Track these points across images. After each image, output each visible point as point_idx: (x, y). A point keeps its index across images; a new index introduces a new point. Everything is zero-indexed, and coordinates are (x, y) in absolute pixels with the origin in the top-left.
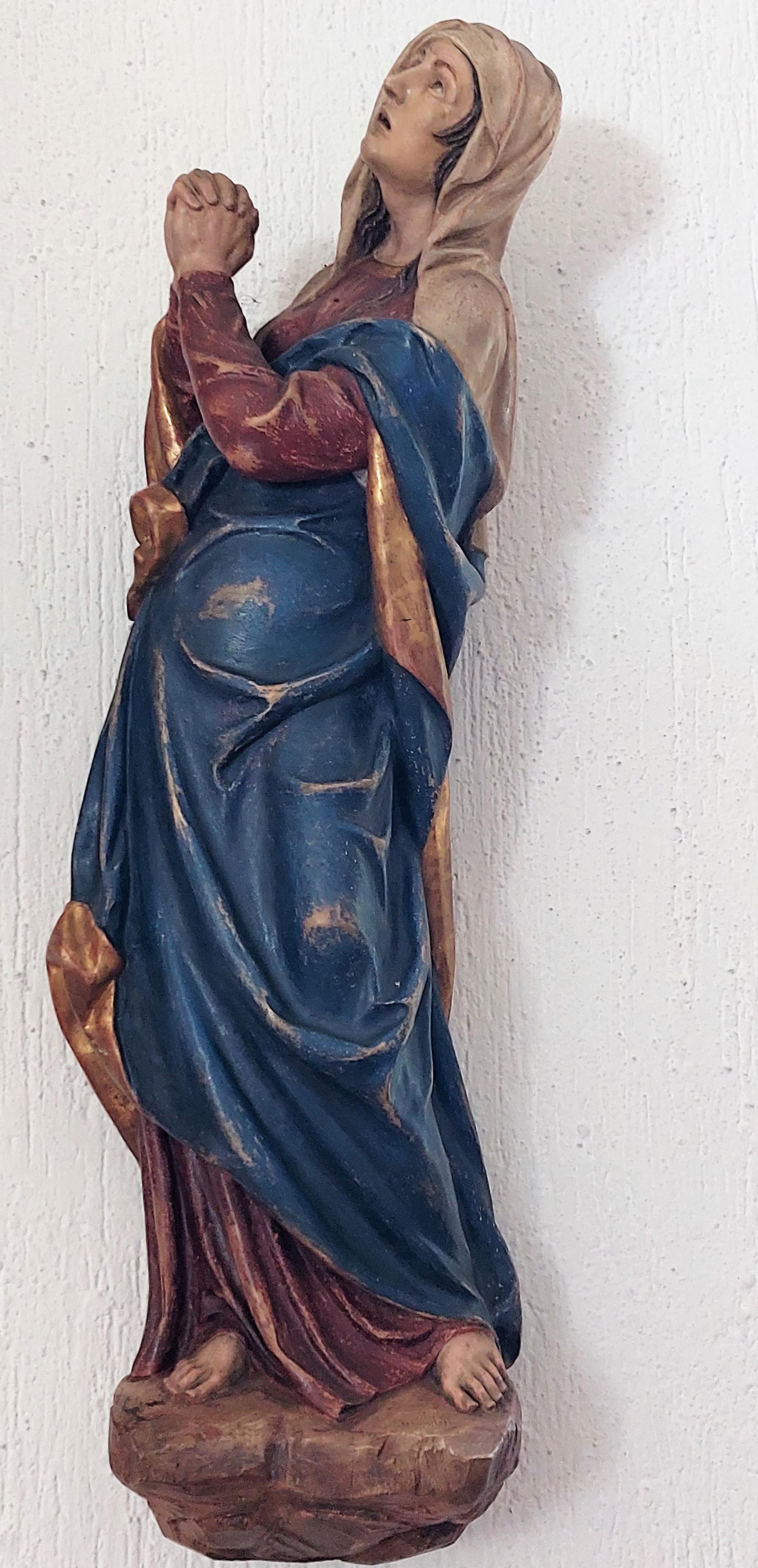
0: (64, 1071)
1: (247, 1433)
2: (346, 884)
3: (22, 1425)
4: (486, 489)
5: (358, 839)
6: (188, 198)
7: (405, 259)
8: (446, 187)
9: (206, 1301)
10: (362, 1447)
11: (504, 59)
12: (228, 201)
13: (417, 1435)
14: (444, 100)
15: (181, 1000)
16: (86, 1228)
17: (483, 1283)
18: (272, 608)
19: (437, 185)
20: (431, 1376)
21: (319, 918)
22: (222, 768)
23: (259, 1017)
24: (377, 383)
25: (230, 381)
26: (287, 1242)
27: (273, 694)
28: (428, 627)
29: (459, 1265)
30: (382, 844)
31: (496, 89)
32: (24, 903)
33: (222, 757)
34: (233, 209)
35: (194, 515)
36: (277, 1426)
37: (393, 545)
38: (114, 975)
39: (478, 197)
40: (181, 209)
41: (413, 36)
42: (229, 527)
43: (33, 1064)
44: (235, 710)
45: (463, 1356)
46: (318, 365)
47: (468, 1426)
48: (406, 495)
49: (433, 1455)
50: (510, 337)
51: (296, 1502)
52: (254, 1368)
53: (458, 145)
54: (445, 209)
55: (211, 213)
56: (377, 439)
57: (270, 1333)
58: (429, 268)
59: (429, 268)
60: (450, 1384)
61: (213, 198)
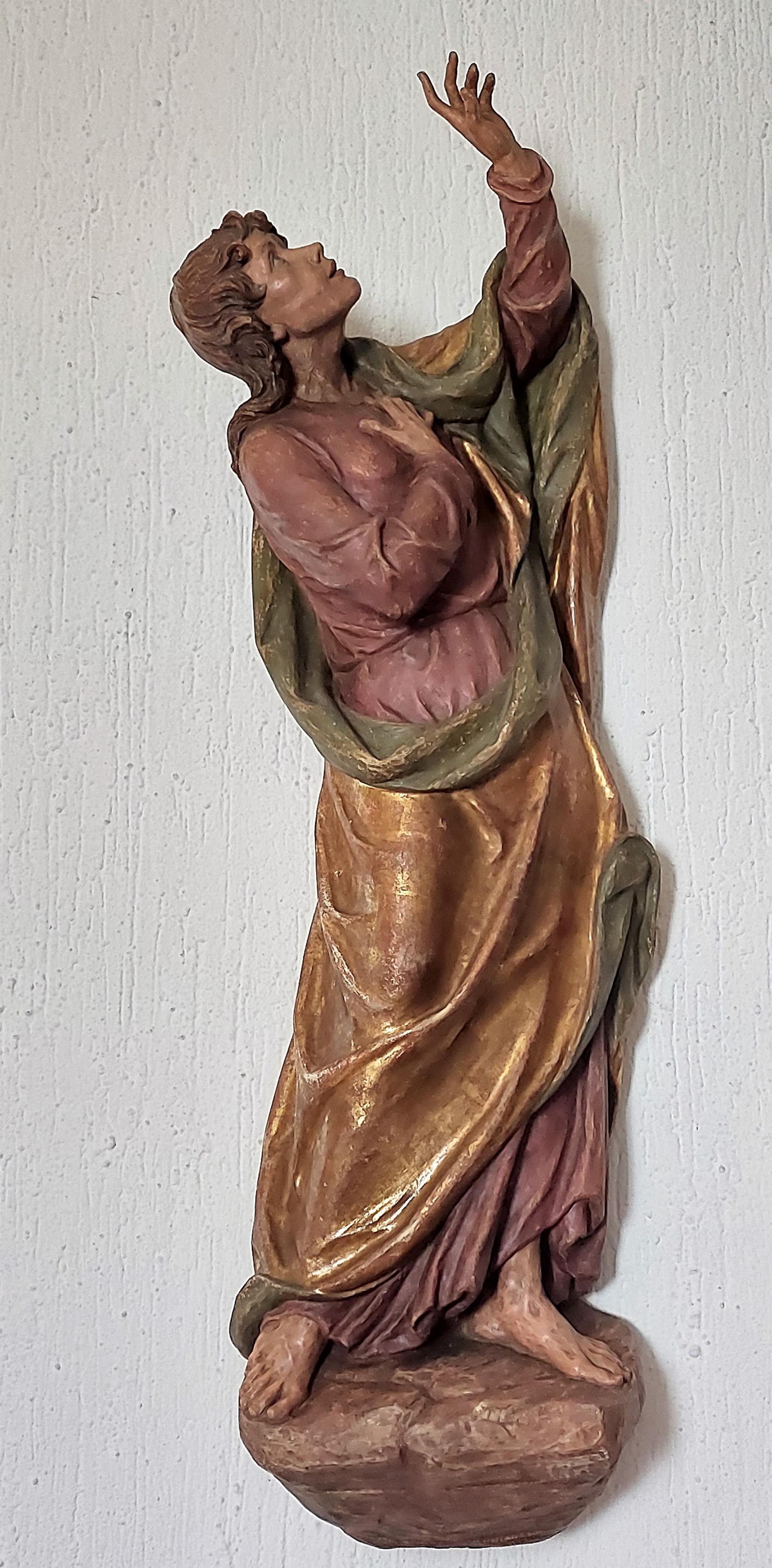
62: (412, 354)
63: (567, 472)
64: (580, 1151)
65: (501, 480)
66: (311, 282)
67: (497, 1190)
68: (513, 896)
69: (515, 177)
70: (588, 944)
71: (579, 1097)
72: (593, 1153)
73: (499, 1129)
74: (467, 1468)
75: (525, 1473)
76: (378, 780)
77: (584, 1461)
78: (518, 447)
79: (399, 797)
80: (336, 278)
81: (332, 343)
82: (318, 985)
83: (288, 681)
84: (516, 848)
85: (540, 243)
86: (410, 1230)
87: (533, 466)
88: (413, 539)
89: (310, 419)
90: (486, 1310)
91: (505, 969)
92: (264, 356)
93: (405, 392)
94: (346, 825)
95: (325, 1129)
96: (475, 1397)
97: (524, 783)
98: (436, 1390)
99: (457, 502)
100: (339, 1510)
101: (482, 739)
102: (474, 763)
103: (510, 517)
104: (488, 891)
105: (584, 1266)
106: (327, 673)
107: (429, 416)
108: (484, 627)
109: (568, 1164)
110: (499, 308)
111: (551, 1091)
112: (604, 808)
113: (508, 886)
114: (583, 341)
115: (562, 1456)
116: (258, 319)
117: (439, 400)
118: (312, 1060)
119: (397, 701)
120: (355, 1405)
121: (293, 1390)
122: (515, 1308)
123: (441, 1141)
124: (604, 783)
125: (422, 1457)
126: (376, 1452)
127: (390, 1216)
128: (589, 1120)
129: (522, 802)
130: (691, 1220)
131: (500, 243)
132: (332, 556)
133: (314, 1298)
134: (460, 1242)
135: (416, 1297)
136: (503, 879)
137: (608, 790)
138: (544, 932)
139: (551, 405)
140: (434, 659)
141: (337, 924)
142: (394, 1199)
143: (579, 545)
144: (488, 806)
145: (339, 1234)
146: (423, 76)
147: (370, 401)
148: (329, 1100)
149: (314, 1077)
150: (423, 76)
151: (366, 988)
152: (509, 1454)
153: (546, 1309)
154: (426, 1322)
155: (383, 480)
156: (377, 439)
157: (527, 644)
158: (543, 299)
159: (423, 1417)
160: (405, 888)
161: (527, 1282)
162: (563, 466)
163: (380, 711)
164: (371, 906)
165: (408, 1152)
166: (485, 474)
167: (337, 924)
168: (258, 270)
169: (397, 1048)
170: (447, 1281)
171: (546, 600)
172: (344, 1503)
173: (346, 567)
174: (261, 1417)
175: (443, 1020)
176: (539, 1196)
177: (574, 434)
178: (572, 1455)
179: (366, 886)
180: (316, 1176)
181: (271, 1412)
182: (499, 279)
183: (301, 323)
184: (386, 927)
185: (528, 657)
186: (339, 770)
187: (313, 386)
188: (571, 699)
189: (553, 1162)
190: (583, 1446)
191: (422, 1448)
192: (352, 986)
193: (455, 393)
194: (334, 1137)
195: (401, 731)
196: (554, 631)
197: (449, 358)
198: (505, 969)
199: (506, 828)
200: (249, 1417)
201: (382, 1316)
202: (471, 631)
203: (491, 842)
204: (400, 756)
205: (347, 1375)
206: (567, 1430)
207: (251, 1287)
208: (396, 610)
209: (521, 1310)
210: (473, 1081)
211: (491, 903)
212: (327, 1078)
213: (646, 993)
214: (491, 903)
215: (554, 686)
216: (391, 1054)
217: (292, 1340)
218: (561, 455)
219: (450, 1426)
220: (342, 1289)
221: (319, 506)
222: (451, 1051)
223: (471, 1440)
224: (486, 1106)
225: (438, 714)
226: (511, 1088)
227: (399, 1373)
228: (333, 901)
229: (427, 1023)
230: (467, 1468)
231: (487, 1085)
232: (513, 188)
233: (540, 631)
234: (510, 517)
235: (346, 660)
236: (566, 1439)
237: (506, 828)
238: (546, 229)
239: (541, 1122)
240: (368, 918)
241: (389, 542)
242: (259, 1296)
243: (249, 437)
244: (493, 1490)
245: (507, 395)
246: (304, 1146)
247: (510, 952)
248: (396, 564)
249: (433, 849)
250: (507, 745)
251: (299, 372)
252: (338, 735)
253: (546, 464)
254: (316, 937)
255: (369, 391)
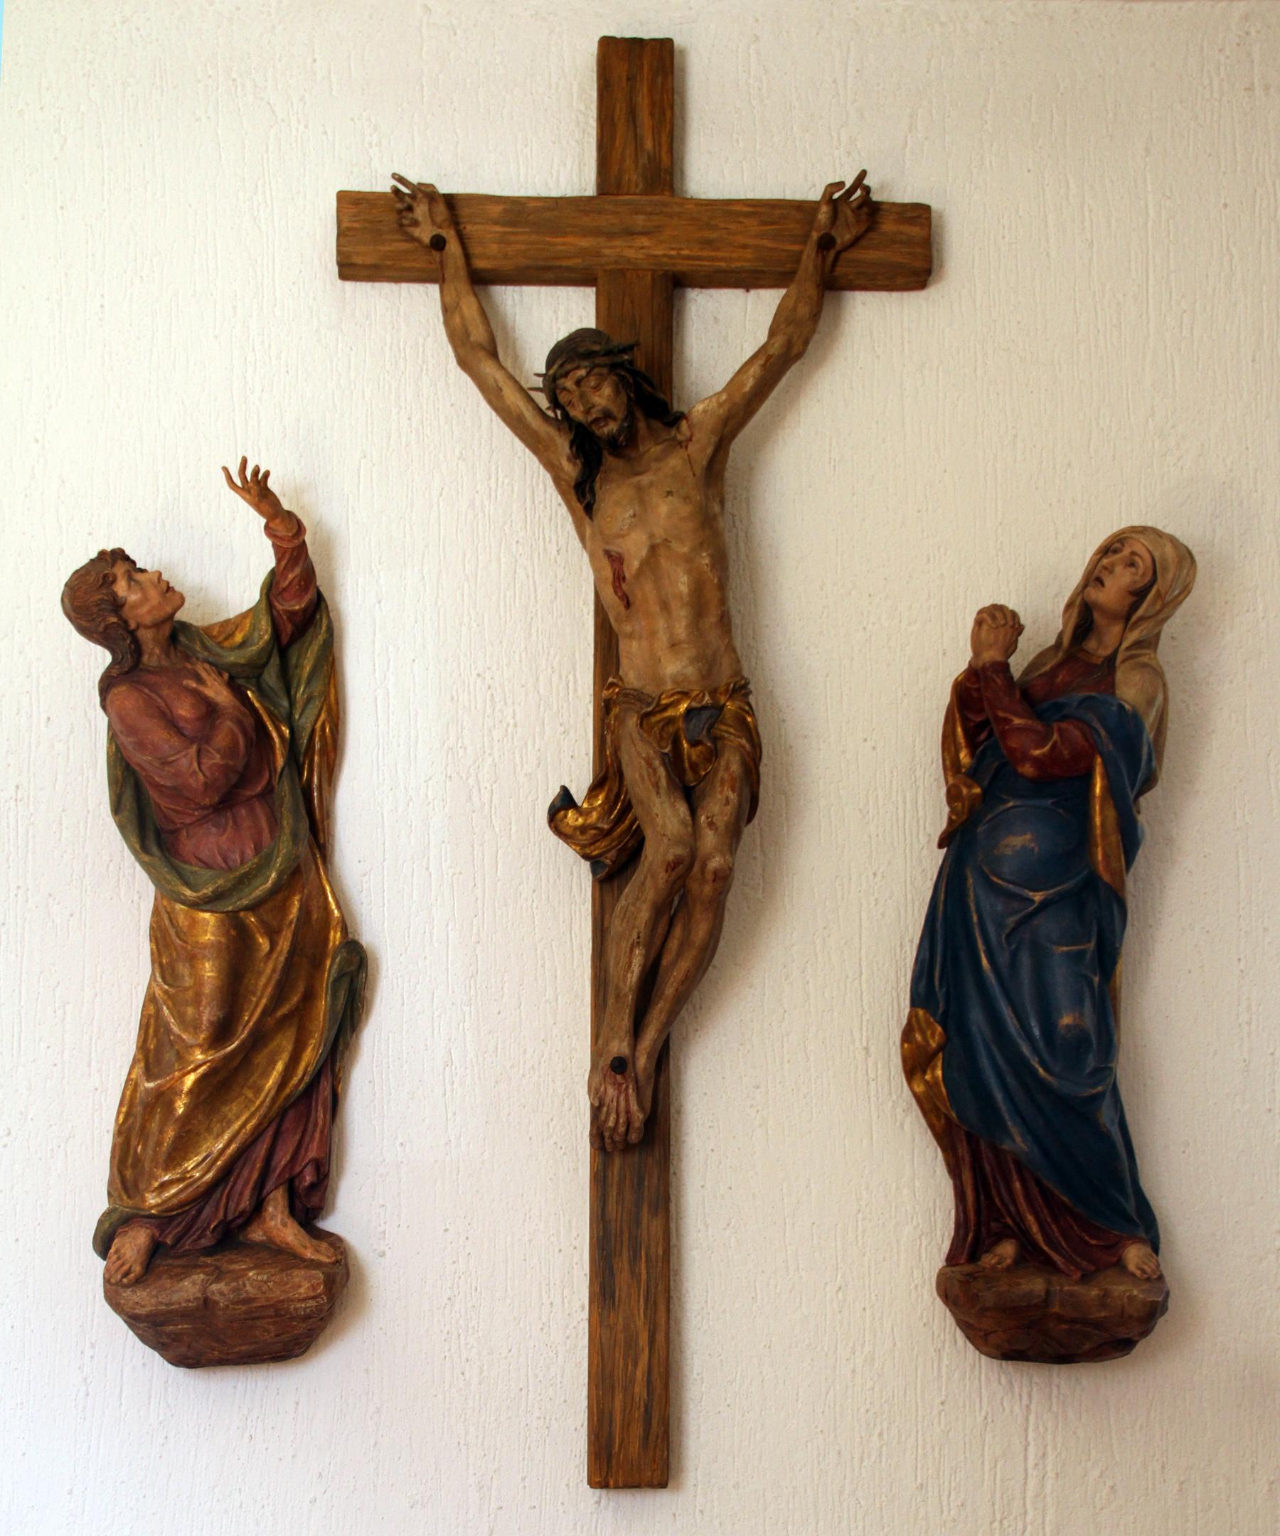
0: (890, 1104)
1: (1035, 1285)
2: (1079, 1002)
3: (873, 1298)
4: (1150, 782)
5: (1086, 977)
6: (990, 622)
7: (1105, 652)
8: (1134, 618)
9: (993, 1225)
10: (1094, 1292)
11: (1169, 550)
12: (1011, 623)
13: (1122, 1288)
14: (1136, 574)
15: (985, 1062)
16: (905, 1191)
17: (1143, 1222)
18: (1036, 850)
19: (1127, 617)
20: (1120, 1265)
21: (1066, 1020)
22: (1008, 936)
23: (1034, 1073)
24: (1103, 733)
25: (1019, 729)
26: (1045, 1192)
27: (1038, 897)
28: (1120, 860)
29: (1131, 1207)
30: (1096, 979)
31: (1165, 569)
32: (866, 1008)
33: (1008, 930)
34: (1013, 627)
35: (989, 797)
36: (1049, 1282)
37: (1101, 816)
38: (941, 1048)
39: (1151, 623)
40: (985, 627)
41: (1115, 529)
42: (1011, 804)
43: (873, 1099)
44: (1015, 905)
45: (1134, 1255)
46: (1065, 718)
47: (1146, 1286)
48: (1110, 789)
49: (1131, 1299)
50: (1166, 699)
51: (1060, 1319)
52: (1030, 1256)
53: (1138, 587)
54: (1132, 629)
55: (1002, 630)
56: (1099, 760)
57: (1039, 1238)
58: (1123, 662)
59: (1123, 662)
60: (1132, 1267)
61: (1003, 622)
62: (215, 633)
63: (312, 711)
64: (314, 1131)
65: (270, 714)
66: (154, 596)
67: (263, 1152)
68: (276, 977)
69: (282, 532)
70: (323, 1004)
71: (315, 1104)
72: (322, 1132)
73: (265, 1116)
74: (244, 1308)
75: (278, 1312)
76: (196, 905)
77: (312, 1303)
78: (282, 694)
79: (207, 915)
80: (169, 594)
81: (167, 630)
82: (151, 1030)
83: (134, 840)
84: (279, 948)
85: (297, 571)
86: (210, 1175)
87: (292, 704)
88: (217, 759)
89: (152, 679)
90: (254, 1226)
91: (271, 1021)
92: (124, 639)
93: (211, 659)
94: (172, 932)
95: (158, 1116)
96: (250, 1269)
97: (283, 908)
98: (225, 1266)
99: (245, 733)
100: (165, 1340)
101: (260, 880)
102: (254, 895)
103: (277, 740)
104: (260, 974)
105: (315, 1200)
106: (158, 834)
107: (226, 676)
108: (260, 811)
109: (307, 1139)
110: (270, 606)
111: (297, 1094)
112: (334, 923)
113: (274, 971)
114: (324, 628)
115: (299, 1300)
116: (120, 618)
117: (235, 665)
118: (149, 1075)
119: (204, 854)
120: (176, 1275)
121: (137, 1269)
122: (273, 1223)
123: (230, 1123)
124: (334, 906)
125: (217, 1303)
126: (189, 1301)
127: (197, 1167)
128: (320, 1115)
129: (283, 919)
130: (381, 1175)
131: (272, 563)
132: (167, 768)
133: (151, 1216)
134: (241, 1182)
135: (212, 1216)
136: (270, 965)
137: (336, 912)
138: (295, 999)
139: (303, 667)
140: (229, 829)
141: (166, 992)
142: (200, 1158)
143: (320, 756)
144: (262, 922)
145: (166, 1178)
146: (226, 470)
147: (189, 666)
148: (163, 1099)
149: (151, 1085)
150: (226, 470)
151: (185, 1030)
152: (268, 1299)
153: (291, 1223)
154: (219, 1229)
155: (198, 719)
156: (196, 693)
157: (287, 823)
158: (299, 603)
159: (217, 1280)
160: (209, 970)
161: (280, 1208)
162: (310, 706)
163: (194, 861)
164: (188, 982)
165: (209, 1130)
166: (262, 711)
167: (166, 992)
168: (121, 588)
169: (204, 1067)
170: (232, 1205)
171: (299, 792)
172: (168, 1335)
173: (177, 775)
174: (119, 1283)
175: (233, 1051)
176: (288, 1157)
177: (317, 687)
178: (305, 1300)
179: (183, 969)
180: (151, 1143)
181: (125, 1280)
182: (272, 587)
183: (148, 620)
184: (198, 995)
185: (287, 830)
186: (165, 894)
187: (153, 655)
188: (314, 855)
189: (297, 1137)
190: (312, 1294)
191: (217, 1297)
192: (176, 1029)
193: (243, 661)
194: (163, 1123)
195: (206, 874)
196: (304, 812)
197: (239, 638)
198: (271, 1021)
199: (273, 935)
200: (111, 1284)
201: (191, 1227)
202: (252, 811)
203: (264, 943)
204: (208, 890)
205: (170, 1261)
206: (303, 1287)
207: (107, 1215)
208: (207, 801)
209: (278, 1223)
210: (249, 1088)
211: (263, 980)
212: (160, 1086)
213: (357, 1038)
214: (263, 980)
215: (303, 849)
216: (201, 1070)
217: (134, 1243)
218: (309, 700)
219: (234, 1284)
220: (167, 1210)
221: (159, 735)
222: (237, 1070)
223: (247, 1292)
224: (258, 1103)
225: (231, 863)
226: (273, 1092)
227: (203, 1259)
228: (163, 978)
229: (223, 1052)
230: (244, 1308)
231: (258, 1090)
232: (281, 539)
233: (295, 812)
234: (277, 740)
235: (171, 827)
236: (302, 1290)
237: (273, 935)
238: (301, 563)
239: (291, 1114)
240: (186, 989)
241: (204, 761)
242: (115, 1217)
243: (115, 691)
244: (258, 1323)
245: (275, 661)
246: (143, 1127)
247: (275, 1009)
248: (208, 774)
249: (228, 947)
250: (274, 884)
251: (144, 647)
252: (169, 877)
253: (299, 706)
254: (151, 999)
255: (187, 658)
